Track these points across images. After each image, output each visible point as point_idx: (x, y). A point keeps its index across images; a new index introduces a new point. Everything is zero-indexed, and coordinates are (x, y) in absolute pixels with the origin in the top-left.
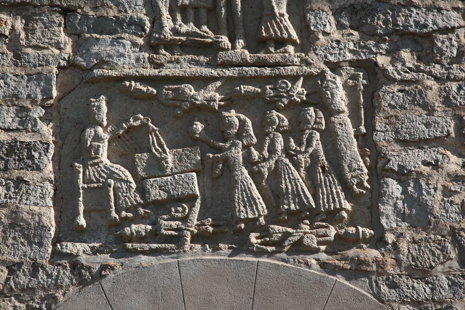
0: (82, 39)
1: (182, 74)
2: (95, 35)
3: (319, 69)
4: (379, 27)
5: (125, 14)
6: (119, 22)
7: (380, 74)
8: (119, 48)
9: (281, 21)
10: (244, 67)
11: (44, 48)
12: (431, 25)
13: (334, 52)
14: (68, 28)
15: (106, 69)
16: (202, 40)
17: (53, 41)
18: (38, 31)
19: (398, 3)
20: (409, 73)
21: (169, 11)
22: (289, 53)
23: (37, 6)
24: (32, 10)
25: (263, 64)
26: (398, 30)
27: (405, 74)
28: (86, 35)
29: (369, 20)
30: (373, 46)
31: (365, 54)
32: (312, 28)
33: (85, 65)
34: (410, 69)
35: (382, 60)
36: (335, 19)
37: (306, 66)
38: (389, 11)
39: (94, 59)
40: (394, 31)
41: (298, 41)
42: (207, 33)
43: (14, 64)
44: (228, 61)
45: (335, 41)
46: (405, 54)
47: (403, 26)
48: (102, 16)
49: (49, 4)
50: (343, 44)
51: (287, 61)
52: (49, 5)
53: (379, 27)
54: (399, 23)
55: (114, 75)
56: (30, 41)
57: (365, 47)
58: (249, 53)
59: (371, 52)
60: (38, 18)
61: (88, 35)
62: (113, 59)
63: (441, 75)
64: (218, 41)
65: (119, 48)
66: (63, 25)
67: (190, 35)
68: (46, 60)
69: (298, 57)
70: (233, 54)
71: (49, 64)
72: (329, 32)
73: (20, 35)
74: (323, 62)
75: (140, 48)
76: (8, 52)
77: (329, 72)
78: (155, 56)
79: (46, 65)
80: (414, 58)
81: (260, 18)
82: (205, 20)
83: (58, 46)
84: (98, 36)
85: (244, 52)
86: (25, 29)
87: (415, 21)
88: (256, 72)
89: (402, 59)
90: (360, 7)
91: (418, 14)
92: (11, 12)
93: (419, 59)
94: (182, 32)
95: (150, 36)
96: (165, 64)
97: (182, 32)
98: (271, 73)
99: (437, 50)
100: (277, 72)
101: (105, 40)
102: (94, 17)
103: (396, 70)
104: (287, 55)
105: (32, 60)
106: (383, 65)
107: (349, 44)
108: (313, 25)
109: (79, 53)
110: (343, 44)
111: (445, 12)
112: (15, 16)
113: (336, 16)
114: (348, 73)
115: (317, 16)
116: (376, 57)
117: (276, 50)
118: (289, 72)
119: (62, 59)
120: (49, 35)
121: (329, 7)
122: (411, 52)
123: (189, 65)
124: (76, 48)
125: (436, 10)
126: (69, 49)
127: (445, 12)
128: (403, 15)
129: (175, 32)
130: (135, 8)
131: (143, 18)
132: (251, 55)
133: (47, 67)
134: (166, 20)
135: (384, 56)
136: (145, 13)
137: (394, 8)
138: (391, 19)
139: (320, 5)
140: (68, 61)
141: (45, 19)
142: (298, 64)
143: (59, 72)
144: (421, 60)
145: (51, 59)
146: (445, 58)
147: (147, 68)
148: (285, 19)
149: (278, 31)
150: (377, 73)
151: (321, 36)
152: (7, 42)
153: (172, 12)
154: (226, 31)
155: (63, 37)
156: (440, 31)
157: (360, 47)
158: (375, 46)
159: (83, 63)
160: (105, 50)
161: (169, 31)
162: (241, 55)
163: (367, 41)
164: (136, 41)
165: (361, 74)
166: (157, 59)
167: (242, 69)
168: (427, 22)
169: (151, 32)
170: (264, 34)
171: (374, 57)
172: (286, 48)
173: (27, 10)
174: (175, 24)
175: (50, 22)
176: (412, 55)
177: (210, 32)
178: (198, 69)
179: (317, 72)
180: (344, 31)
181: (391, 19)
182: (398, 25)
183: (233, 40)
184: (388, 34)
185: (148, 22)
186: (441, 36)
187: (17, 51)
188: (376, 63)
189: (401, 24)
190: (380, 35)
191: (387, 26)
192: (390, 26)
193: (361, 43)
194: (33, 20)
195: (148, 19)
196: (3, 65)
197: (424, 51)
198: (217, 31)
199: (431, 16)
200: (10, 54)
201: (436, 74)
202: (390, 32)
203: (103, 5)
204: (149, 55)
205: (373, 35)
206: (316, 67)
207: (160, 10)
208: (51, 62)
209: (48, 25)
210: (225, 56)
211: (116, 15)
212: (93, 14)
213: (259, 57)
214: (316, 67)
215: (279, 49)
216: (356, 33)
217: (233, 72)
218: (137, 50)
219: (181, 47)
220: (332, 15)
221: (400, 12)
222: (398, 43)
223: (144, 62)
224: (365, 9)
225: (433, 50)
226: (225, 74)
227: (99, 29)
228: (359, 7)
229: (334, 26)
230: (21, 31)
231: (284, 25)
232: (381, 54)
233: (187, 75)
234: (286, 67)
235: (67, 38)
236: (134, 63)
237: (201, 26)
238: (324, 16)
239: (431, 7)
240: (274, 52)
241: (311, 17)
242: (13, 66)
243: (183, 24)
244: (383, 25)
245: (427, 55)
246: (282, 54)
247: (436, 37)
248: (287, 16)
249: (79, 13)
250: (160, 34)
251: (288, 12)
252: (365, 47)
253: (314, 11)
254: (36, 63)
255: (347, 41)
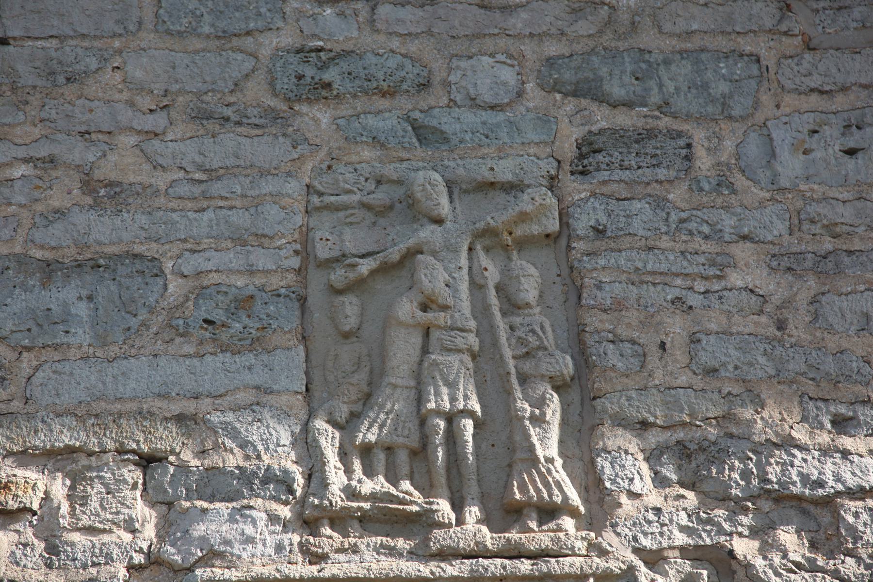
0: (175, 511)
1: (362, 573)
2: (199, 503)
3: (623, 562)
4: (734, 485)
5: (257, 462)
6: (245, 477)
7: (741, 574)
8: (244, 527)
9: (549, 471)
10: (480, 559)
11: (104, 531)
12: (831, 483)
13: (650, 530)
14: (150, 491)
15: (220, 567)
16: (401, 507)
17: (121, 517)
18: (94, 499)
19: (767, 440)
20: (795, 573)
21: (339, 454)
22: (566, 531)
23: (95, 452)
24: (84, 461)
25: (516, 553)
26: (769, 491)
27: (789, 575)
28: (183, 503)
29: (714, 471)
30: (725, 520)
31: (709, 535)
32: (608, 484)
33: (180, 562)
34: (798, 565)
35: (744, 548)
36: (651, 468)
37: (600, 558)
38: (750, 454)
39: (196, 547)
40: (762, 492)
41: (582, 509)
42: (411, 495)
43: (45, 564)
44: (449, 547)
45: (652, 509)
46: (787, 536)
47: (779, 482)
48: (213, 468)
49: (117, 448)
50: (666, 515)
51: (561, 548)
52: (117, 451)
53: (734, 485)
54: (770, 476)
55: (234, 579)
56: (79, 519)
57: (709, 521)
58: (491, 532)
59: (721, 531)
60: (94, 474)
61: (186, 504)
62: (232, 547)
63: (856, 578)
64: (431, 509)
65: (244, 527)
66: (140, 487)
67: (379, 499)
68: (107, 554)
69: (583, 539)
70: (459, 535)
71: (112, 561)
72: (640, 492)
73: (59, 508)
74: (630, 549)
75: (284, 526)
76: (36, 542)
77: (643, 569)
78: (311, 539)
79: (106, 564)
80: (803, 544)
81: (510, 466)
82: (405, 470)
83: (130, 527)
84: (205, 505)
85: (480, 531)
86: (69, 497)
87: (800, 474)
88: (504, 568)
89: (781, 545)
90: (696, 447)
91: (805, 461)
92: (45, 465)
93: (814, 546)
94: (363, 494)
95: (304, 502)
96: (331, 555)
97: (363, 494)
98: (532, 570)
99: (846, 530)
100: (544, 568)
101: (218, 512)
102: (199, 470)
103: (771, 566)
104: (561, 535)
105: (79, 556)
106: (745, 557)
107: (678, 515)
108: (610, 479)
109: (169, 537)
110: (666, 515)
111: (856, 459)
112: (53, 473)
113: (652, 462)
114: (679, 572)
115: (616, 462)
116: (731, 540)
117: (541, 524)
118: (566, 568)
119: (136, 551)
120: (114, 505)
121: (638, 445)
122: (798, 532)
123: (376, 556)
124: (164, 530)
125: (838, 455)
126: (150, 532)
127: (856, 459)
128: (777, 463)
129: (351, 493)
130: (276, 451)
131: (290, 470)
132: (494, 535)
133: (108, 566)
134: (334, 470)
135: (746, 540)
136: (294, 459)
137: (759, 450)
138: (754, 470)
139: (620, 442)
140: (148, 555)
141: (108, 475)
142: (584, 552)
143: (130, 577)
144: (817, 548)
145: (115, 552)
146: (863, 545)
147: (296, 564)
148: (555, 468)
149: (544, 491)
150: (734, 572)
151: (624, 499)
152: (35, 522)
153: (344, 455)
154: (445, 491)
155: (141, 510)
156: (849, 493)
157: (700, 520)
158: (729, 519)
159: (176, 557)
160: (218, 532)
161: (339, 493)
162: (475, 535)
163: (713, 510)
164: (276, 513)
165: (705, 573)
166: (315, 546)
167: (477, 562)
168: (823, 477)
169: (305, 495)
170: (518, 496)
171: (726, 541)
172: (560, 521)
173: (75, 461)
174: (350, 479)
175: (117, 481)
176: (800, 537)
177: (416, 493)
178: (394, 564)
179: (620, 569)
180: (667, 490)
181: (754, 470)
182: (769, 481)
183: (458, 507)
184: (752, 498)
185: (300, 476)
186: (852, 503)
187: (53, 539)
188: (731, 553)
189: (775, 480)
190: (737, 500)
191: (748, 483)
192: (755, 482)
193: (702, 514)
194: (84, 479)
195: (301, 470)
196: (24, 566)
197: (821, 532)
198: (428, 490)
199: (829, 465)
200: (40, 546)
201: (848, 575)
202: (755, 494)
203: (216, 447)
204: (301, 538)
205: (724, 499)
206: (618, 559)
207: (323, 454)
208: (115, 557)
209: (112, 487)
210: (444, 538)
211: (241, 464)
212: (198, 463)
213: (508, 540)
214: (618, 559)
215: (546, 523)
216: (690, 495)
217: (460, 568)
218: (279, 528)
219: (361, 521)
220: (644, 459)
221: (772, 457)
222: (770, 515)
223: (290, 552)
224: (705, 450)
225: (838, 528)
226: (444, 572)
227: (209, 491)
228: (693, 447)
229: (649, 481)
230: (62, 501)
231: (553, 478)
232: (740, 535)
233: (373, 576)
234: (561, 559)
235: (147, 510)
236: (273, 554)
237: (398, 481)
238: (629, 461)
239: (829, 449)
240: (536, 529)
241: (604, 463)
242: (44, 567)
243: (365, 478)
244: (742, 479)
245: (828, 539)
246: (552, 534)
247: (842, 506)
248: (559, 462)
249: (172, 464)
250: (321, 499)
251: (561, 454)
252: (709, 521)
253: (609, 453)
254: (87, 560)
255: (674, 510)
